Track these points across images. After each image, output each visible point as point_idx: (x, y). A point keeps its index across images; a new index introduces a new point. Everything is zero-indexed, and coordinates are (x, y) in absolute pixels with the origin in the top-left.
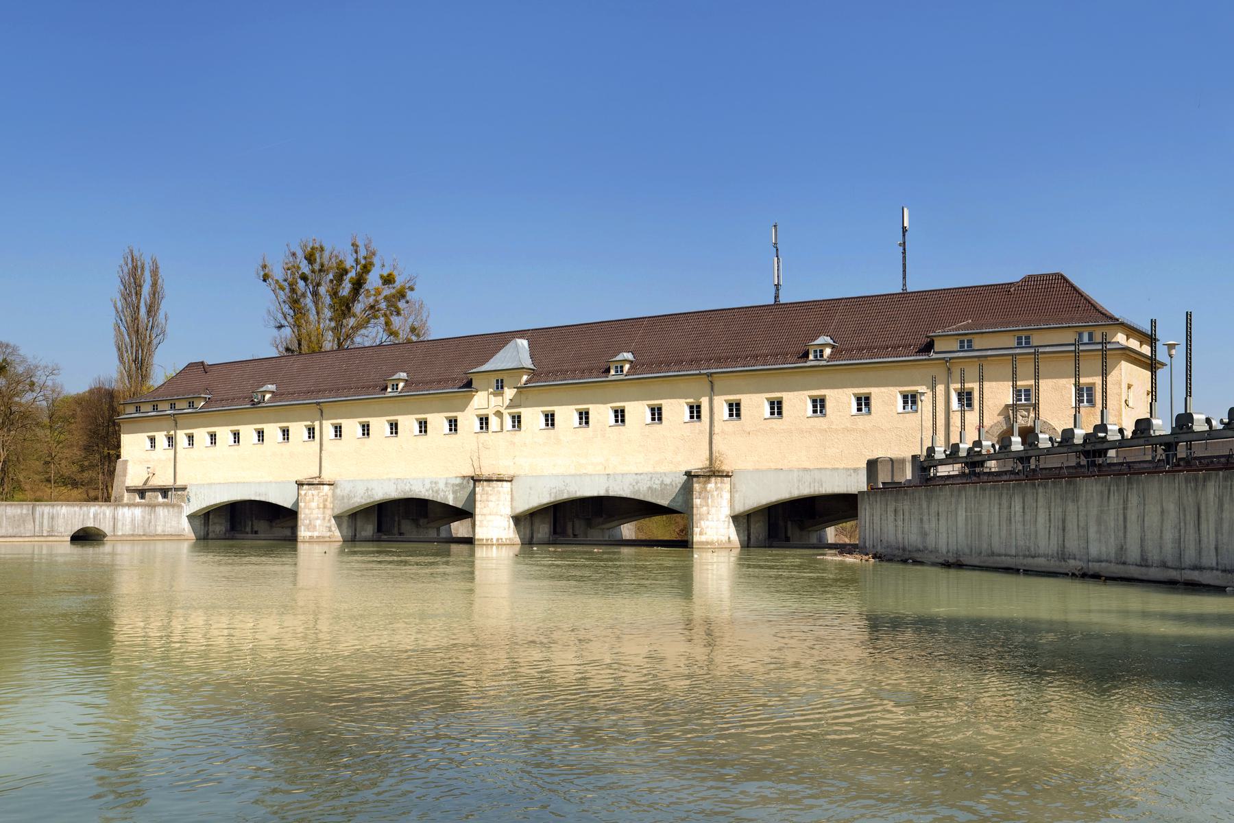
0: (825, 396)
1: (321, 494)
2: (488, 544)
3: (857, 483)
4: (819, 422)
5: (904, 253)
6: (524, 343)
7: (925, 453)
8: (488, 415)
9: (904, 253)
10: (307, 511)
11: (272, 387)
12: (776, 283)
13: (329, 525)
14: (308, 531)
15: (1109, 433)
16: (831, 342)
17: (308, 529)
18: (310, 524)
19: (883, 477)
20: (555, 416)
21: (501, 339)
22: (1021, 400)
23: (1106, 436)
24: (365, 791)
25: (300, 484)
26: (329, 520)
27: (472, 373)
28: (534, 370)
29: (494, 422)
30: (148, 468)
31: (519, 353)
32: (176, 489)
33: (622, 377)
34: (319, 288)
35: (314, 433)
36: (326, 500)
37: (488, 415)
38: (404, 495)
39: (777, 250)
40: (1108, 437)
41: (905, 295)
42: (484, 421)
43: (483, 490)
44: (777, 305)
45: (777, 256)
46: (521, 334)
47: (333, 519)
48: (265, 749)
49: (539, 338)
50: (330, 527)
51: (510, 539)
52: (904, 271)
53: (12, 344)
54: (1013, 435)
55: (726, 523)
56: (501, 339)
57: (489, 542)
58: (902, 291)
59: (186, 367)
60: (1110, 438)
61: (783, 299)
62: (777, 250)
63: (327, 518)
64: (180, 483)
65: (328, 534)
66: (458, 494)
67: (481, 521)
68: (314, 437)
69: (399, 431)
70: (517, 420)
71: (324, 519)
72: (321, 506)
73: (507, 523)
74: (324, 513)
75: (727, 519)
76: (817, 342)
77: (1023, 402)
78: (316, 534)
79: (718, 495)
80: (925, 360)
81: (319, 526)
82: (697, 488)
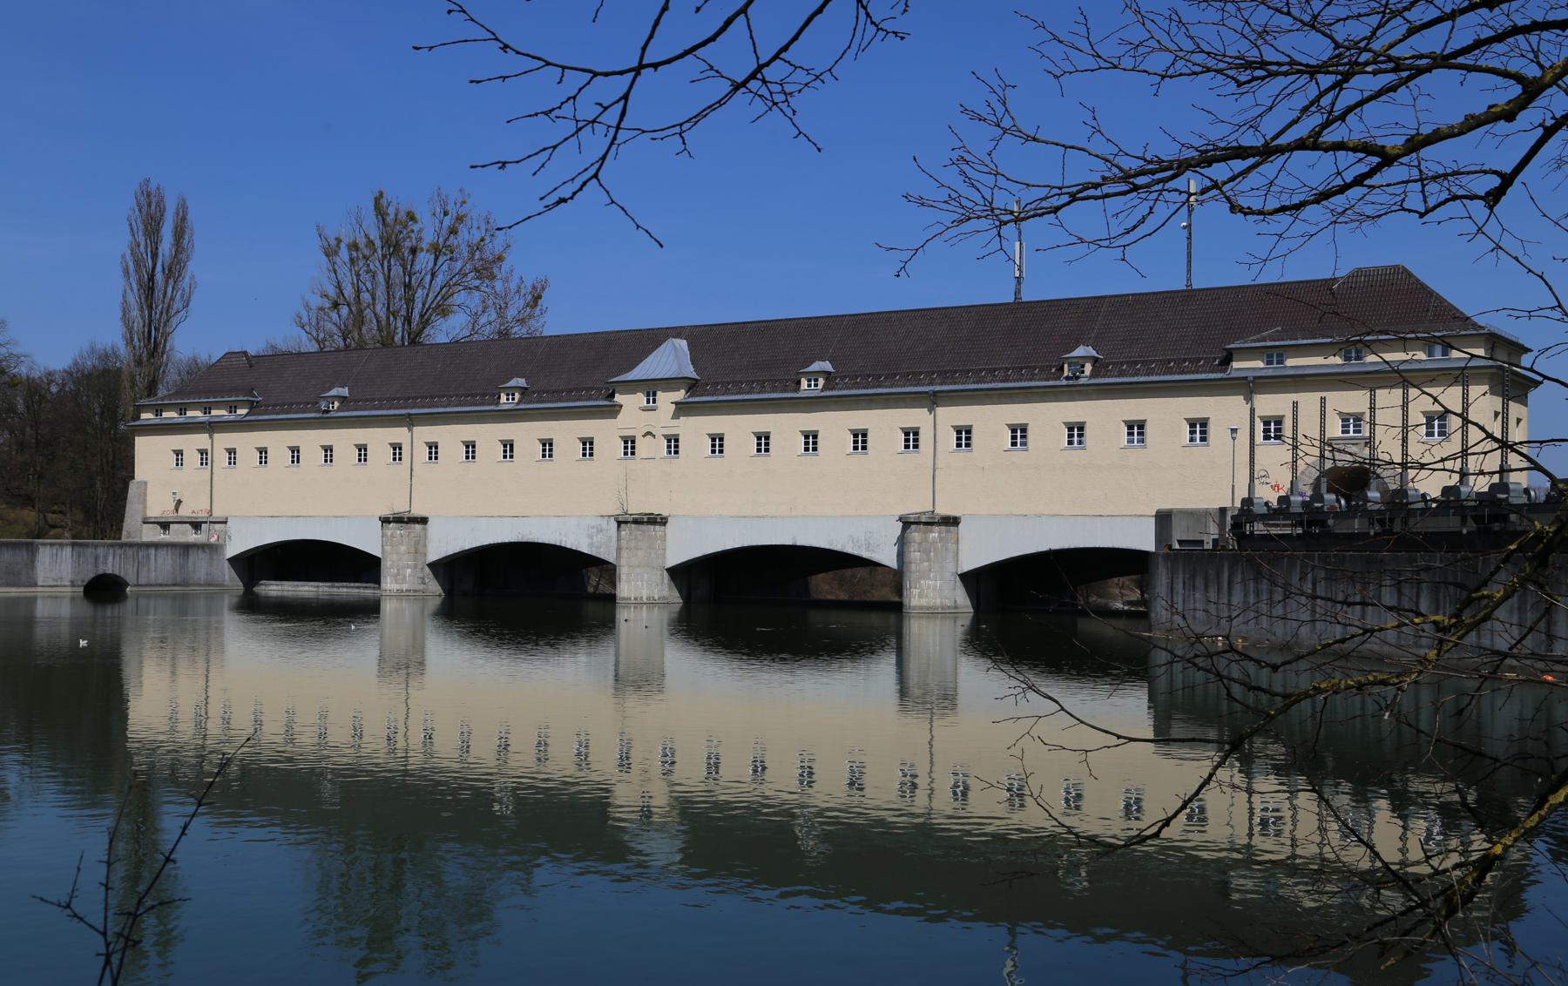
1: (413, 535)
2: (628, 603)
3: (1143, 539)
4: (1076, 455)
5: (1189, 238)
6: (683, 344)
7: (1238, 504)
8: (635, 437)
9: (1189, 238)
10: (395, 557)
12: (1017, 275)
13: (421, 575)
14: (396, 583)
15: (1512, 494)
16: (1094, 353)
17: (396, 580)
19: (1178, 533)
20: (869, 435)
21: (650, 340)
22: (1348, 432)
23: (1507, 498)
24: (70, 561)
25: (907, 523)
26: (422, 569)
27: (611, 382)
28: (697, 380)
29: (642, 445)
30: (174, 493)
31: (672, 359)
33: (816, 394)
36: (419, 543)
37: (635, 437)
38: (523, 538)
39: (1020, 233)
40: (1510, 499)
41: (1189, 295)
42: (629, 444)
44: (1018, 303)
45: (1020, 241)
46: (677, 332)
49: (703, 339)
50: (423, 578)
51: (664, 598)
52: (1189, 262)
53: (427, 668)
54: (1369, 490)
55: (952, 582)
56: (650, 340)
57: (639, 601)
58: (1185, 288)
59: (222, 358)
60: (1513, 501)
61: (1027, 296)
62: (1020, 233)
63: (420, 566)
64: (218, 513)
65: (422, 587)
67: (629, 575)
68: (206, 464)
69: (514, 454)
70: (673, 443)
71: (415, 567)
72: (412, 550)
73: (659, 577)
75: (952, 578)
76: (1074, 354)
77: (1351, 434)
78: (405, 587)
79: (942, 547)
80: (1221, 379)
81: (409, 576)
82: (932, 535)
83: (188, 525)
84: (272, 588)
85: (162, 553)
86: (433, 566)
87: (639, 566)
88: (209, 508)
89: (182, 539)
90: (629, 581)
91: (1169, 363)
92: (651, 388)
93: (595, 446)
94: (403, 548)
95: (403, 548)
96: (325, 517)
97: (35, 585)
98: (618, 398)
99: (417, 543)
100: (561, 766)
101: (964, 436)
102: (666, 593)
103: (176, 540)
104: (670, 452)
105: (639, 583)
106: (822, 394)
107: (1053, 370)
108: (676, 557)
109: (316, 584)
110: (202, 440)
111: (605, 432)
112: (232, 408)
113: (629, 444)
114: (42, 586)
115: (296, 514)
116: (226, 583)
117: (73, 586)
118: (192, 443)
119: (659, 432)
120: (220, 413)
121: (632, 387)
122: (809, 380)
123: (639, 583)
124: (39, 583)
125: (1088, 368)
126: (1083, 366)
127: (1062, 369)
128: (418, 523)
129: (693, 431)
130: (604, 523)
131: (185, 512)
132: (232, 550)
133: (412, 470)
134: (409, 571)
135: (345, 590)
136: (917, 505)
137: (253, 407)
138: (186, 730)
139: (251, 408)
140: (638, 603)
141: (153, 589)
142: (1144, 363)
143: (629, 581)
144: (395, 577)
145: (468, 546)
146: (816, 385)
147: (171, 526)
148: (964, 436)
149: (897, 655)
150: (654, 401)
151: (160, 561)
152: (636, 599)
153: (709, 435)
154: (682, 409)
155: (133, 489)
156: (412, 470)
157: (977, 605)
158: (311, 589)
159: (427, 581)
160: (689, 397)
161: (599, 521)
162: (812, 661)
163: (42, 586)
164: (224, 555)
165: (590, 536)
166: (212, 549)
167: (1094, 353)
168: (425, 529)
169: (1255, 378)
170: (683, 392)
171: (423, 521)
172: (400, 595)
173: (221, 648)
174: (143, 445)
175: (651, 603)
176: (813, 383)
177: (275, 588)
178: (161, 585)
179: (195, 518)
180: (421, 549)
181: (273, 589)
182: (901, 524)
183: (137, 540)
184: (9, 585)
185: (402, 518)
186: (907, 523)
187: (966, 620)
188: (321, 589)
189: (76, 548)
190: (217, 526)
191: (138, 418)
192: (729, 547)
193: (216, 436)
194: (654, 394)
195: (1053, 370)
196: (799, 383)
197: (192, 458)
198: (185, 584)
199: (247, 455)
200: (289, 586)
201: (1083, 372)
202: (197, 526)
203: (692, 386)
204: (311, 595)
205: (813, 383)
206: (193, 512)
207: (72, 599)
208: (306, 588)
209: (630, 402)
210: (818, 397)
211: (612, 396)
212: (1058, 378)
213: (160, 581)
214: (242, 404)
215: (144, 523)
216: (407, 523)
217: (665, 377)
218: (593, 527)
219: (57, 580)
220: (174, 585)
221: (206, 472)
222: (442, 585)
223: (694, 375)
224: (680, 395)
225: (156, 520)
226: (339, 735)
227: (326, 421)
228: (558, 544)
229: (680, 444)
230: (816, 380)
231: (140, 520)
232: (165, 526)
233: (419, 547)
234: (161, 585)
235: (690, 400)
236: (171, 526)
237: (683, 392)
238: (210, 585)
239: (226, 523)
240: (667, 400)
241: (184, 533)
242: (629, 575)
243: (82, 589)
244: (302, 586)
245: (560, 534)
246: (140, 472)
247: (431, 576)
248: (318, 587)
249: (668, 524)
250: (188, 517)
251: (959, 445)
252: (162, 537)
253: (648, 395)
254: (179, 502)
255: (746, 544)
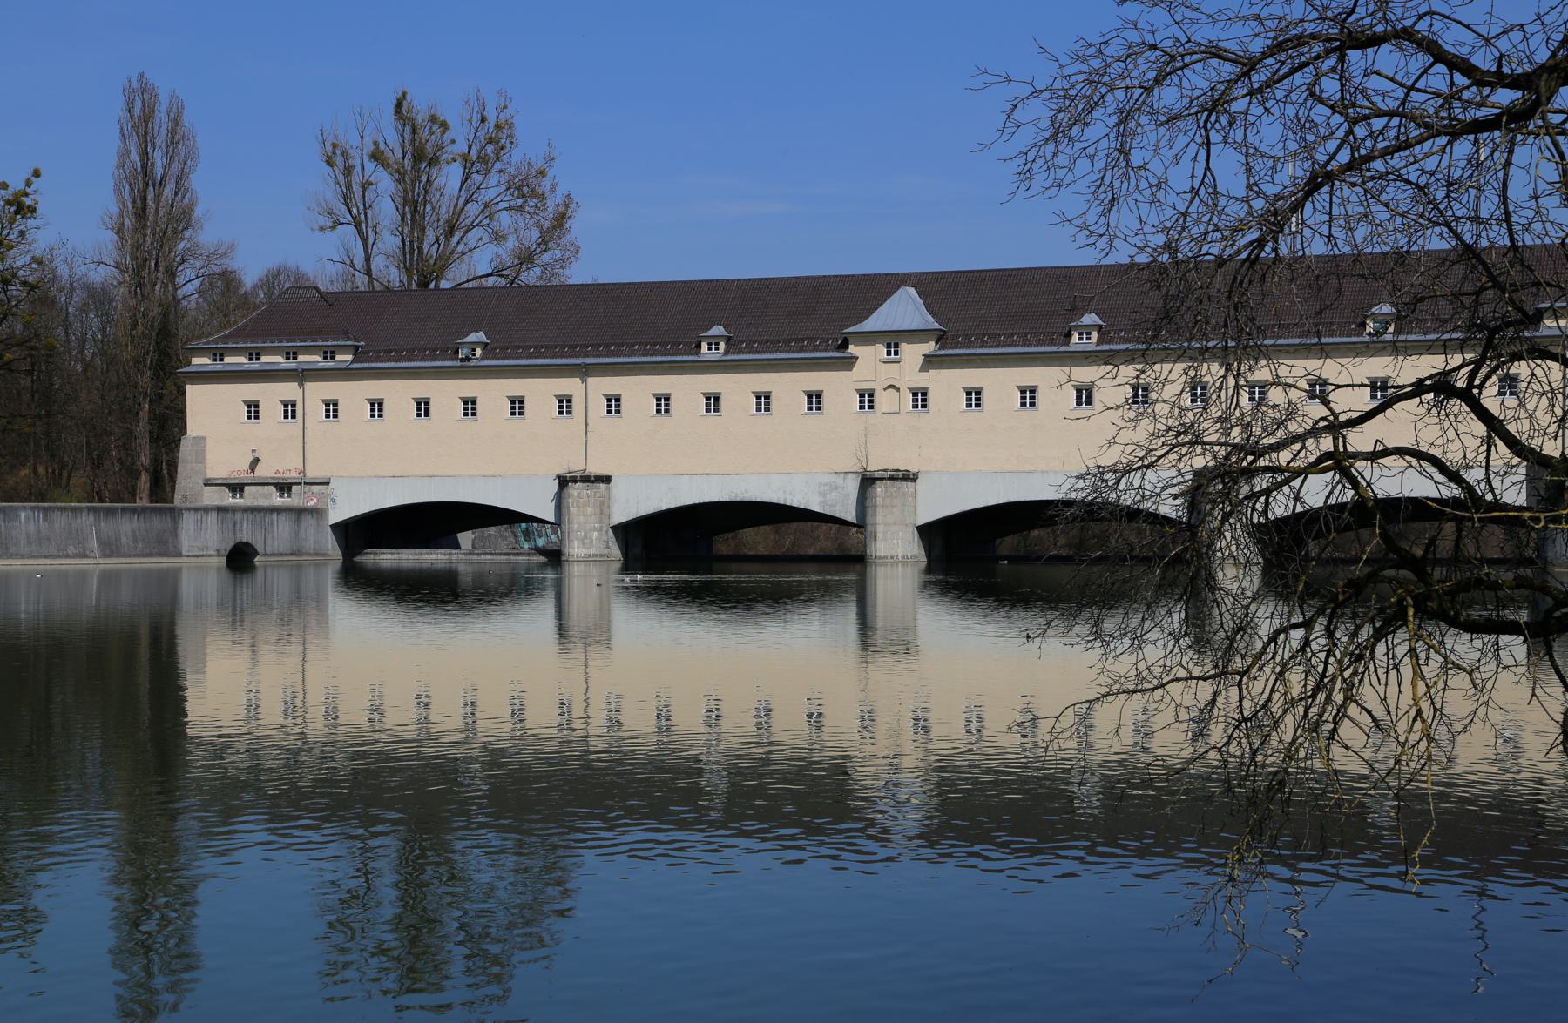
0: (927, 388)
1: (598, 495)
2: (884, 561)
10: (582, 519)
11: (480, 336)
18: (586, 537)
20: (525, 402)
21: (877, 288)
25: (564, 481)
26: (607, 532)
29: (883, 400)
30: (253, 451)
32: (586, 479)
34: (434, 170)
35: (294, 411)
42: (867, 399)
43: (886, 491)
47: (610, 531)
48: (15, 811)
49: (933, 288)
51: (915, 556)
56: (877, 288)
63: (605, 529)
64: (311, 474)
66: (828, 496)
67: (885, 533)
68: (294, 417)
70: (921, 398)
71: (601, 530)
74: (601, 522)
78: (592, 551)
83: (272, 487)
84: (384, 556)
85: (283, 517)
86: (615, 528)
87: (895, 524)
88: (301, 467)
89: (263, 503)
90: (885, 539)
91: (646, 345)
92: (893, 340)
93: (261, 409)
94: (590, 510)
95: (590, 510)
96: (470, 476)
97: (180, 555)
98: (853, 349)
99: (602, 504)
100: (790, 731)
101: (614, 403)
102: (916, 551)
103: (256, 504)
104: (970, 406)
105: (895, 541)
106: (724, 358)
107: (1353, 326)
108: (621, 515)
109: (448, 551)
110: (289, 390)
111: (838, 386)
112: (329, 354)
113: (867, 399)
114: (188, 556)
115: (430, 474)
116: (329, 552)
117: (219, 556)
118: (271, 395)
119: (904, 387)
120: (306, 359)
121: (870, 338)
122: (710, 344)
123: (895, 541)
124: (184, 553)
125: (479, 352)
126: (474, 350)
127: (1363, 325)
128: (603, 482)
129: (948, 384)
130: (839, 480)
131: (262, 472)
132: (340, 512)
133: (587, 425)
134: (595, 533)
135: (488, 557)
136: (575, 465)
137: (358, 353)
138: (272, 715)
139: (355, 354)
140: (894, 561)
141: (285, 558)
142: (582, 346)
143: (885, 539)
144: (584, 541)
145: (664, 507)
146: (717, 349)
147: (246, 488)
148: (614, 403)
149: (858, 604)
150: (896, 353)
151: (281, 528)
152: (892, 557)
153: (414, 399)
154: (930, 362)
155: (186, 447)
156: (587, 425)
157: (929, 555)
158: (440, 557)
159: (610, 544)
160: (940, 349)
161: (833, 478)
162: (692, 610)
163: (188, 556)
164: (327, 520)
165: (823, 494)
166: (317, 513)
167: (485, 339)
168: (608, 489)
169: (303, 370)
170: (933, 343)
171: (607, 479)
172: (588, 559)
173: (323, 620)
174: (196, 395)
175: (905, 562)
176: (1085, 336)
177: (389, 556)
178: (282, 555)
179: (278, 478)
180: (606, 512)
181: (387, 558)
182: (557, 481)
183: (198, 504)
184: (161, 555)
185: (590, 477)
186: (564, 481)
187: (924, 565)
188: (454, 557)
189: (220, 513)
190: (315, 488)
191: (189, 363)
192: (992, 502)
193: (308, 385)
194: (896, 346)
195: (1353, 326)
196: (699, 346)
197: (272, 410)
198: (298, 553)
199: (272, 410)
200: (441, 554)
201: (474, 355)
202: (284, 488)
203: (941, 338)
204: (441, 565)
205: (1085, 336)
206: (278, 472)
207: (219, 569)
208: (434, 556)
209: (868, 356)
210: (722, 361)
211: (844, 345)
212: (1361, 335)
213: (281, 550)
214: (343, 349)
215: (205, 485)
216: (593, 482)
217: (911, 328)
218: (826, 485)
219: (202, 550)
220: (292, 554)
221: (294, 427)
222: (621, 550)
223: (937, 326)
224: (930, 347)
225: (225, 482)
226: (689, 720)
227: (467, 370)
228: (782, 502)
229: (340, 408)
230: (717, 344)
231: (201, 482)
232: (237, 488)
233: (603, 509)
234: (282, 555)
235: (942, 352)
236: (246, 488)
237: (933, 343)
238: (317, 554)
239: (328, 484)
240: (913, 353)
241: (269, 496)
242: (885, 533)
243: (225, 559)
244: (428, 554)
245: (785, 492)
246: (194, 426)
247: (614, 539)
248: (450, 554)
249: (918, 481)
250: (273, 478)
251: (1023, 404)
252: (277, 500)
253: (889, 346)
254: (256, 461)
255: (1013, 499)
